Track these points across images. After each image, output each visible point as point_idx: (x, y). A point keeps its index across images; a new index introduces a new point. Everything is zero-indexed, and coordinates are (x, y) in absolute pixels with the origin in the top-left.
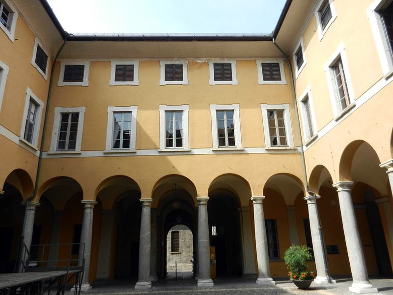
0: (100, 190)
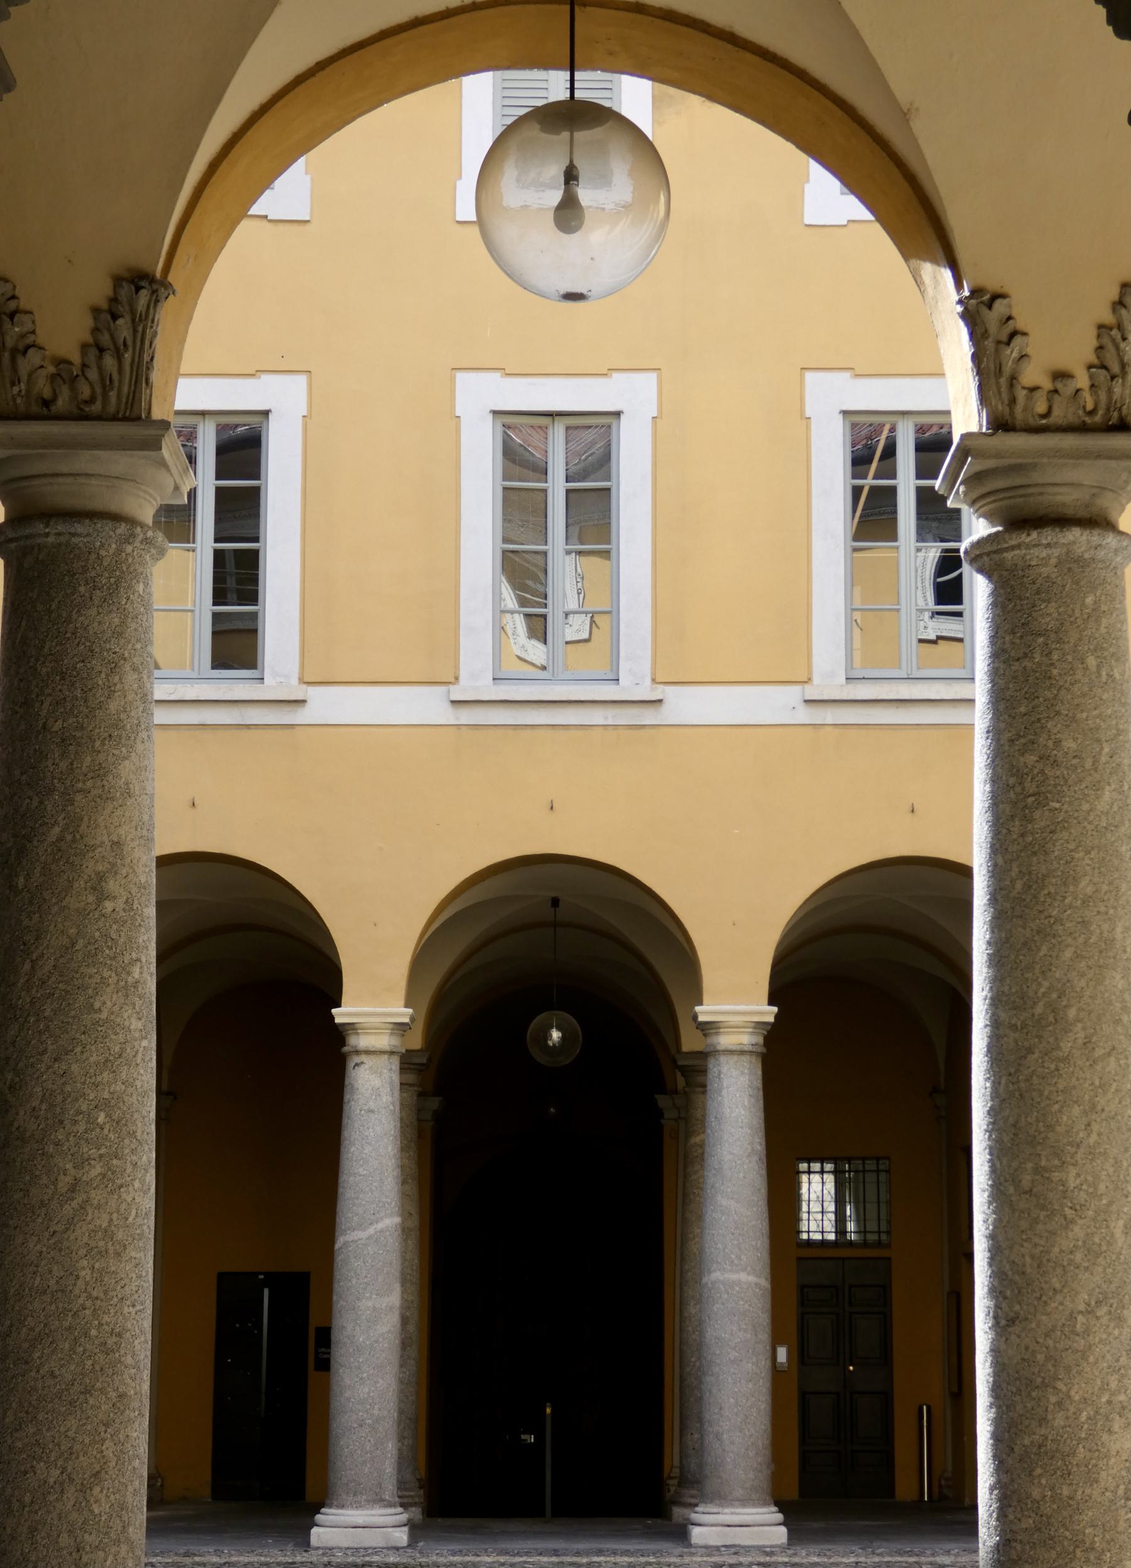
0: (426, 937)
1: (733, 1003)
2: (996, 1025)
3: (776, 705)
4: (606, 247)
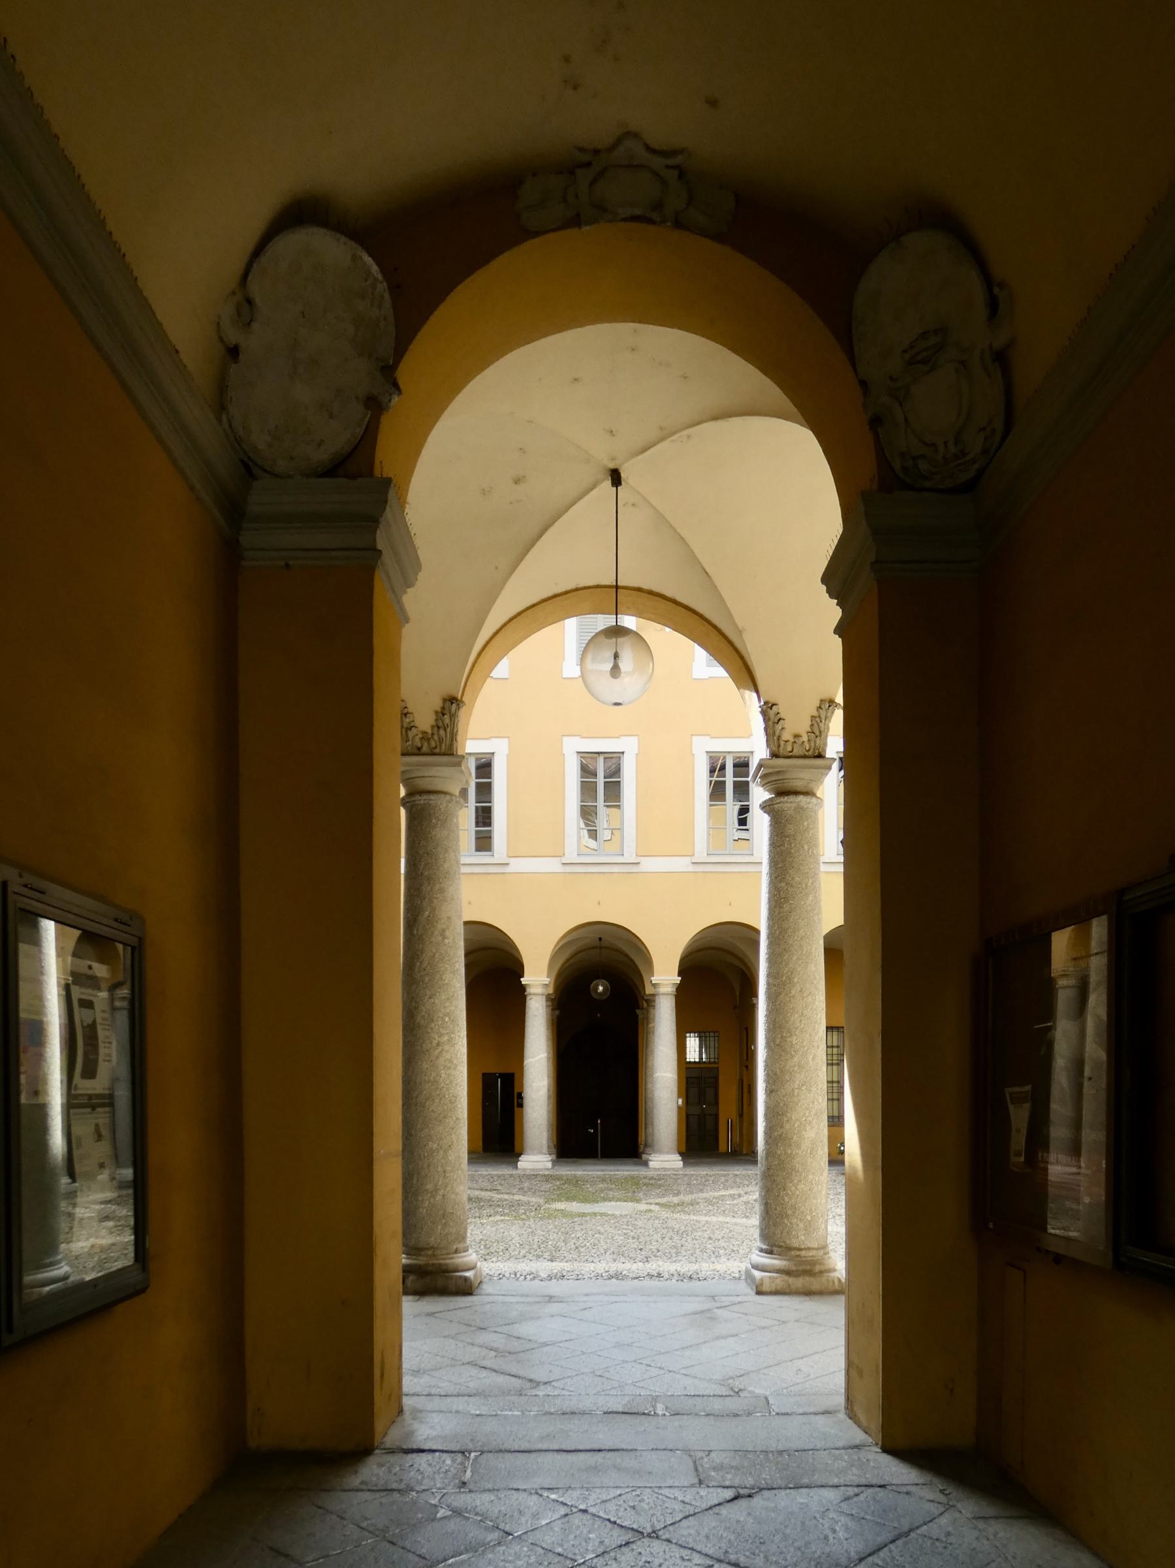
1: (664, 977)
2: (769, 985)
3: (681, 864)
4: (630, 683)
